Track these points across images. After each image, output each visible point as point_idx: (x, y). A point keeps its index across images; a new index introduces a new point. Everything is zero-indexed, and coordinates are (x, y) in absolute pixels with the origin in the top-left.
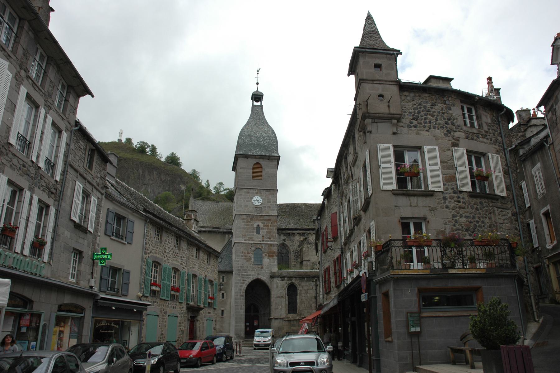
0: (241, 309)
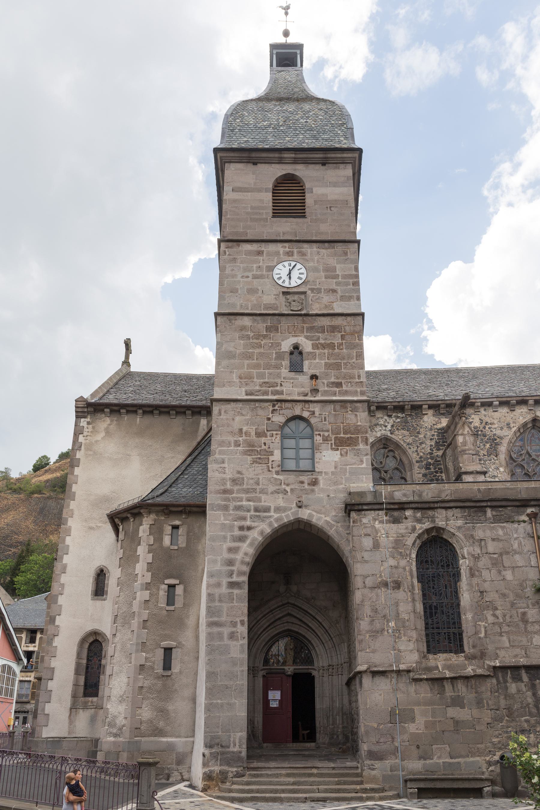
0: (232, 636)
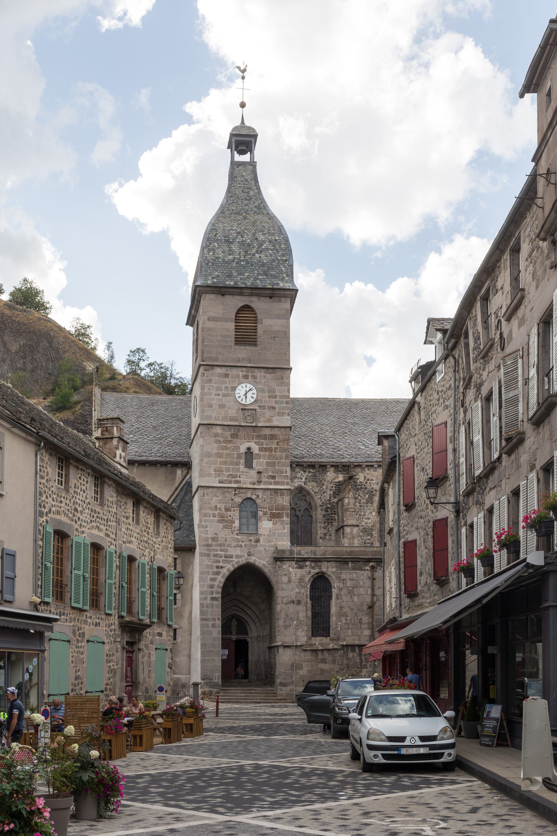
0: (213, 626)
